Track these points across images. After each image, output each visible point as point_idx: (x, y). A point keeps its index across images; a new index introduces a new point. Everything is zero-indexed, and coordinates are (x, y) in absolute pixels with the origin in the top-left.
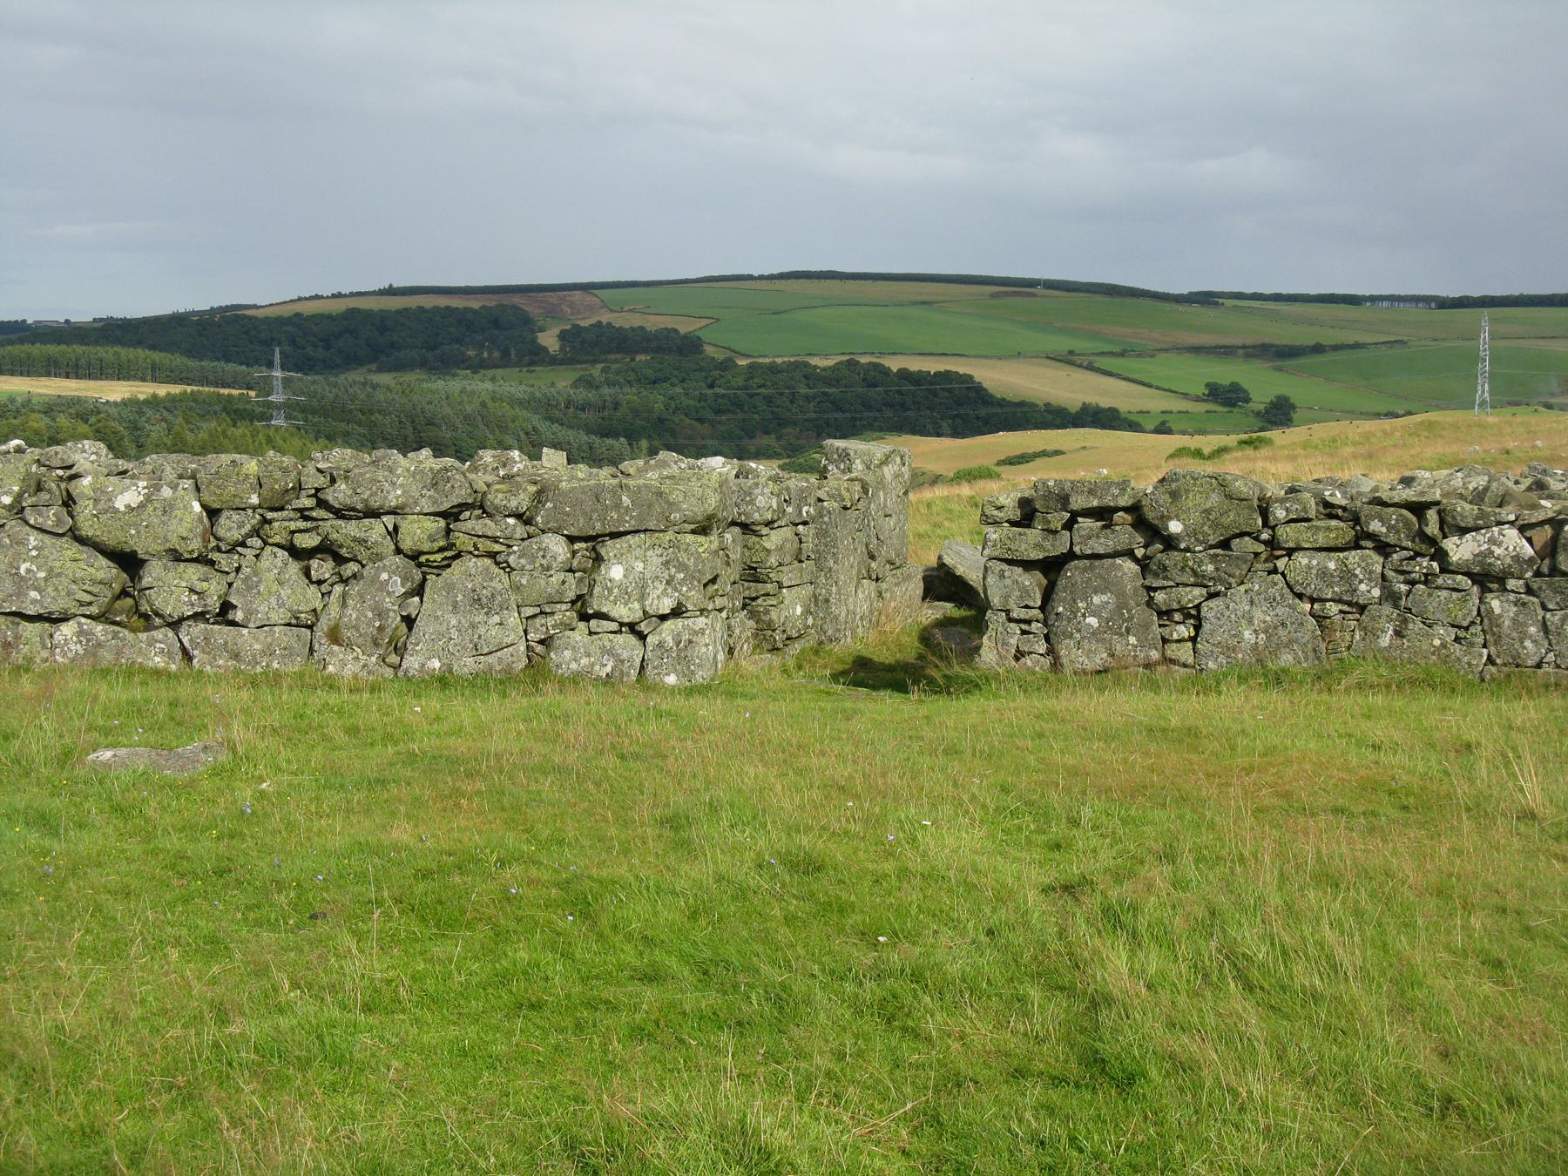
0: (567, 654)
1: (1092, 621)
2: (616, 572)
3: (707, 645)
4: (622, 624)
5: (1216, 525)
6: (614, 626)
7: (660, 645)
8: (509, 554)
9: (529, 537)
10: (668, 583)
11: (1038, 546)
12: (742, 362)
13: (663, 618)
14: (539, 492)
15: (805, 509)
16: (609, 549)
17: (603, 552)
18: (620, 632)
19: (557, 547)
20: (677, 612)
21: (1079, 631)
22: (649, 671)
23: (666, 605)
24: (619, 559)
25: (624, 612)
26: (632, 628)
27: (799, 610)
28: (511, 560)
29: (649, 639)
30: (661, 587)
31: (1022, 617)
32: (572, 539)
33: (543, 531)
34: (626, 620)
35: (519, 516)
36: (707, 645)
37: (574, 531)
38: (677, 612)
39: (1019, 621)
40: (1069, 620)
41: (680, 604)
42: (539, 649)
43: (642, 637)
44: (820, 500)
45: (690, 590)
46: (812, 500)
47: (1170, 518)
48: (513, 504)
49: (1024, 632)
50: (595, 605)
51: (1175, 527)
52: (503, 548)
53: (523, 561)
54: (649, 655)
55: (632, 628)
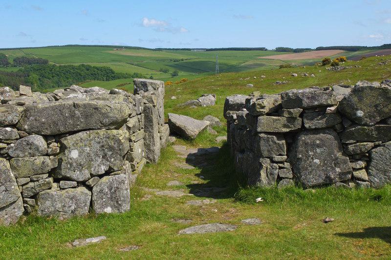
0: (48, 203)
1: (317, 161)
2: (75, 154)
3: (127, 189)
4: (78, 182)
5: (380, 113)
6: (75, 183)
7: (101, 191)
8: (9, 149)
9: (21, 137)
10: (103, 157)
11: (285, 126)
12: (58, 65)
13: (101, 176)
14: (25, 111)
15: (140, 108)
16: (69, 141)
17: (65, 142)
18: (78, 186)
19: (39, 141)
20: (108, 173)
21: (311, 166)
22: (96, 206)
23: (103, 169)
24: (76, 145)
25: (77, 175)
26: (83, 183)
27: (140, 151)
28: (10, 152)
29: (94, 189)
30: (100, 160)
31: (280, 160)
32: (46, 137)
33: (29, 134)
34: (81, 180)
35: (13, 126)
36: (127, 189)
37: (48, 132)
38: (108, 173)
39: (277, 163)
40: (305, 161)
41: (110, 168)
42: (31, 201)
43: (90, 188)
44: (145, 103)
45: (115, 160)
46: (142, 104)
47: (357, 109)
48: (10, 118)
49: (280, 168)
50: (64, 172)
51: (360, 113)
52: (5, 145)
53: (18, 152)
54: (95, 198)
55: (83, 183)
